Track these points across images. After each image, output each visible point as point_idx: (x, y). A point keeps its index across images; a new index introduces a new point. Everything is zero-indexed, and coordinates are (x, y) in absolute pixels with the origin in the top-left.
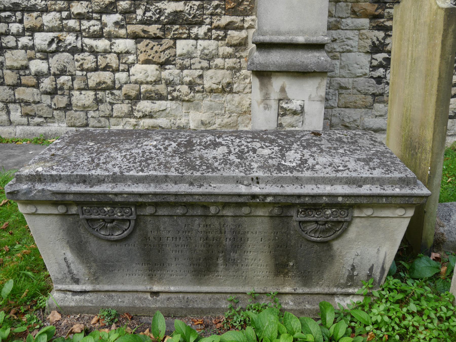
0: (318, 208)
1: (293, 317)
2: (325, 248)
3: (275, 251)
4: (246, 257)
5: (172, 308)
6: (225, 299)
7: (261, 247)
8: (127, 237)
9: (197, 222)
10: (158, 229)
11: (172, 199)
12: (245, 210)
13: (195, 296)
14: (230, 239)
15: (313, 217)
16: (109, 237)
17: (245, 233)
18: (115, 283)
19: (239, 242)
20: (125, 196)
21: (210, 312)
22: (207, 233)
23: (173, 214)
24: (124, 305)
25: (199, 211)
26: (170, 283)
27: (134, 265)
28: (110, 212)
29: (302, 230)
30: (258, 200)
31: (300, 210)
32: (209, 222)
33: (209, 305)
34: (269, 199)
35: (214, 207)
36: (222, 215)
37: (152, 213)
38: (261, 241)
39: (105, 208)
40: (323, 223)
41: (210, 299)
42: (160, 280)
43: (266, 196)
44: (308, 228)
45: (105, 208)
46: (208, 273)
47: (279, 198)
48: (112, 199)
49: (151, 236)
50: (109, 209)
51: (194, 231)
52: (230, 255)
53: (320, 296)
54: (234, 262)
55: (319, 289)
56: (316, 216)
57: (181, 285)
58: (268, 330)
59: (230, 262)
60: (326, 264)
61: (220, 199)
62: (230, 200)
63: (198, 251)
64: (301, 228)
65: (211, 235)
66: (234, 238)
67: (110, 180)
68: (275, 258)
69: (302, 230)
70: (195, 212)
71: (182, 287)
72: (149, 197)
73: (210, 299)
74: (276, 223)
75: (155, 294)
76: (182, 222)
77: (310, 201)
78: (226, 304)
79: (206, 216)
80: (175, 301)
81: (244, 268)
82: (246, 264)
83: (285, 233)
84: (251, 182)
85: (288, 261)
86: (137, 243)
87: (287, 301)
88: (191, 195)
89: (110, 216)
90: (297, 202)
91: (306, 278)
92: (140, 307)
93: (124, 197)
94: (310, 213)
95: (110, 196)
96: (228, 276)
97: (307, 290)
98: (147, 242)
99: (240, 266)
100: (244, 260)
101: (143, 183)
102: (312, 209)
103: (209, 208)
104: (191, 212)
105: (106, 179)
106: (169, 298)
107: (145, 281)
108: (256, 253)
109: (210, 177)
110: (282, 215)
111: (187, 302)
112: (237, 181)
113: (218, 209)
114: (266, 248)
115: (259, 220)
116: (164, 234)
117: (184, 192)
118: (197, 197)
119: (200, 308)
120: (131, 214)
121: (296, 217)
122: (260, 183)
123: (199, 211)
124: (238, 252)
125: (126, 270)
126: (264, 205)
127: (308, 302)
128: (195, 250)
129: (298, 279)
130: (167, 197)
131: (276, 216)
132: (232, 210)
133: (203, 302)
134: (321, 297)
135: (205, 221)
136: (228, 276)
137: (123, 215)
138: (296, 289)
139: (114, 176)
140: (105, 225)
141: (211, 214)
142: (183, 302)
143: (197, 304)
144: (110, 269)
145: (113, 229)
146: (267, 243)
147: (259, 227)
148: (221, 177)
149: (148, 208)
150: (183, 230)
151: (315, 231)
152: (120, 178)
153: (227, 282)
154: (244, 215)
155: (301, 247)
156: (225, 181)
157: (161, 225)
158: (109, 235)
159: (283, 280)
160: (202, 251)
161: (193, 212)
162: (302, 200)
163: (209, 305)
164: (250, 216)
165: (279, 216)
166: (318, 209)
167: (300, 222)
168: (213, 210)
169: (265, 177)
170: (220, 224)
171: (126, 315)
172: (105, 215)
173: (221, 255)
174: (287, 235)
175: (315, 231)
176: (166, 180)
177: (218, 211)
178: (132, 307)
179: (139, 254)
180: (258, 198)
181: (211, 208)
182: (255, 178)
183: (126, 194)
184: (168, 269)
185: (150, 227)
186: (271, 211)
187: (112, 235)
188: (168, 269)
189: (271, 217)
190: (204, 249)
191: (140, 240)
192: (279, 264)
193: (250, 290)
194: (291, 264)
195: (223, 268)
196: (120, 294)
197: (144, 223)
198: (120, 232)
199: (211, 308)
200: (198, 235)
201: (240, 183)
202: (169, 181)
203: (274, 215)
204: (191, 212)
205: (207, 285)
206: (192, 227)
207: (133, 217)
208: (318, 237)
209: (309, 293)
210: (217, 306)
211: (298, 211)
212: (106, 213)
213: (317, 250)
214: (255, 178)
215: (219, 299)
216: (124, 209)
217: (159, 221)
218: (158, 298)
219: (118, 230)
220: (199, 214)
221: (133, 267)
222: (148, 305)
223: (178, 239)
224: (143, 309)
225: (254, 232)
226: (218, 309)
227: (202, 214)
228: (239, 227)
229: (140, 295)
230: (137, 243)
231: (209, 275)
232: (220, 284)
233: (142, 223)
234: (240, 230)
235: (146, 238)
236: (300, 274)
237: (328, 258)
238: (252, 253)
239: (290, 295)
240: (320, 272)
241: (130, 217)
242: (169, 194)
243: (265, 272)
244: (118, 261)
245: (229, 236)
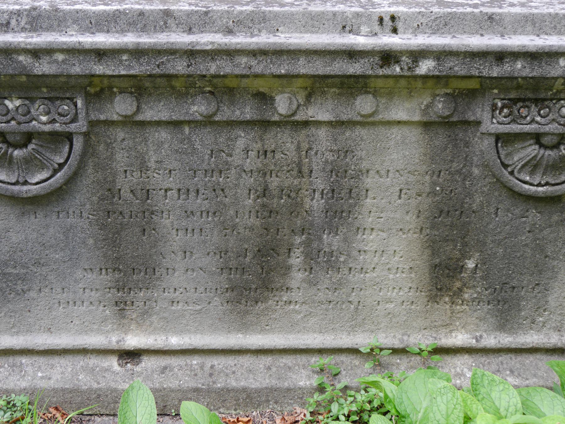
0: (542, 96)
1: (493, 380)
2: (555, 218)
3: (432, 227)
4: (362, 246)
5: (172, 391)
6: (304, 367)
7: (398, 216)
8: (60, 188)
9: (241, 143)
10: (143, 167)
11: (180, 67)
12: (364, 104)
13: (230, 361)
14: (322, 193)
15: (530, 123)
16: (17, 188)
17: (360, 174)
18: (29, 331)
19: (343, 203)
20: (60, 57)
21: (268, 401)
22: (265, 174)
23: (182, 118)
24: (52, 384)
25: (248, 109)
26: (170, 325)
27: (79, 274)
28: (20, 110)
29: (502, 163)
30: (398, 69)
31: (499, 104)
32: (270, 144)
33: (268, 381)
34: (425, 67)
35: (286, 95)
36: (304, 118)
37: (129, 113)
38: (400, 197)
39: (7, 102)
40: (555, 140)
41: (269, 368)
42: (144, 319)
43: (418, 55)
44: (516, 159)
45: (7, 102)
46: (266, 294)
47: (450, 63)
48: (25, 67)
49: (124, 184)
50: (18, 103)
51: (233, 171)
52: (320, 239)
53: (538, 356)
54: (331, 262)
55: (536, 337)
56: (538, 119)
57: (195, 332)
58: (435, 408)
59: (321, 261)
60: (555, 263)
61: (303, 67)
62: (328, 70)
63: (242, 231)
64: (499, 158)
65: (274, 182)
66: (333, 191)
67: (23, 23)
68: (433, 246)
69: (502, 163)
70: (238, 113)
71: (199, 336)
72: (121, 61)
73: (269, 368)
74: (437, 143)
75: (131, 355)
76: (203, 140)
77: (527, 72)
78: (309, 377)
79: (265, 124)
80: (180, 373)
81: (355, 278)
82: (359, 267)
83: (459, 172)
84: (377, 28)
85: (465, 256)
86: (88, 206)
87: (458, 370)
88: (230, 53)
89: (19, 123)
90: (495, 75)
91: (506, 306)
92: (90, 390)
93: (56, 61)
94: (524, 112)
95: (21, 58)
96: (313, 302)
97: (506, 340)
98: (112, 204)
99: (346, 272)
100: (355, 253)
101: (108, 31)
102: (529, 100)
103: (272, 99)
104: (227, 113)
105: (13, 22)
106: (165, 368)
107: (104, 320)
108: (384, 235)
109: (276, 15)
110: (455, 119)
111: (211, 375)
112: (344, 27)
113: (295, 103)
114: (411, 218)
115: (396, 133)
116: (159, 180)
117: (212, 43)
118: (244, 60)
119: (244, 390)
120: (74, 120)
121: (489, 123)
122: (400, 30)
123: (248, 109)
124: (343, 230)
125: (59, 290)
126: (412, 83)
127: (512, 372)
128: (234, 227)
129: (486, 307)
130: (168, 61)
131: (439, 123)
132: (330, 104)
133: (251, 376)
134: (541, 360)
135: (262, 140)
136: (313, 302)
137: (53, 121)
138: (481, 336)
139: (34, 13)
140: (6, 152)
141: (276, 118)
142: (200, 375)
143: (236, 380)
144: (19, 288)
145: (30, 164)
146: (413, 202)
147: (395, 156)
148: (303, 15)
149: (118, 98)
150: (205, 166)
151: (533, 166)
152: (49, 18)
153: (313, 320)
154: (359, 119)
155: (496, 214)
156: (313, 26)
157: (152, 153)
158: (16, 183)
159: (449, 312)
160: (252, 229)
161: (233, 112)
162: (506, 69)
163: (268, 381)
164: (373, 124)
165: (446, 123)
166: (544, 100)
167: (498, 137)
168: (283, 105)
169: (413, 13)
170: (298, 148)
171: (54, 412)
172: (8, 122)
173: (298, 240)
174: (464, 180)
175: (533, 166)
176: (166, 23)
177: (294, 107)
178: (71, 391)
179: (91, 241)
180: (398, 62)
181: (278, 98)
182: (387, 19)
183: (62, 51)
184: (164, 285)
185: (121, 158)
186: (428, 106)
187: (26, 183)
188: (164, 285)
189: (426, 125)
190: (258, 222)
191: (95, 199)
192: (440, 264)
193: (368, 341)
194: (470, 264)
195: (304, 280)
196: (41, 360)
197: (108, 145)
198: (44, 175)
199: (272, 390)
200: (242, 181)
201: (350, 32)
202: (174, 27)
203: (434, 118)
204: (227, 113)
205: (263, 331)
206: (229, 159)
207: (81, 126)
208: (539, 185)
209: (513, 346)
210: (286, 384)
211: (494, 108)
212: (9, 117)
213: (534, 224)
214: (387, 19)
215: (290, 368)
216: (58, 103)
217: (146, 140)
218: (138, 369)
219: (43, 167)
220: (248, 117)
221: (76, 281)
222: (113, 385)
223: (192, 194)
224: (99, 396)
225: (383, 172)
226: (288, 390)
227: (255, 117)
228: (345, 156)
229: (93, 361)
230: (88, 206)
231: (266, 299)
232: (293, 327)
233: (102, 147)
234: (347, 165)
235: (111, 192)
236: (491, 294)
237: (560, 245)
238: (374, 234)
239: (466, 356)
240: (541, 287)
241: (73, 127)
242: (172, 52)
243: (407, 290)
244: (37, 263)
245: (320, 183)
